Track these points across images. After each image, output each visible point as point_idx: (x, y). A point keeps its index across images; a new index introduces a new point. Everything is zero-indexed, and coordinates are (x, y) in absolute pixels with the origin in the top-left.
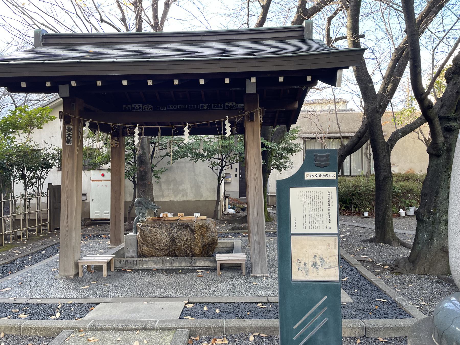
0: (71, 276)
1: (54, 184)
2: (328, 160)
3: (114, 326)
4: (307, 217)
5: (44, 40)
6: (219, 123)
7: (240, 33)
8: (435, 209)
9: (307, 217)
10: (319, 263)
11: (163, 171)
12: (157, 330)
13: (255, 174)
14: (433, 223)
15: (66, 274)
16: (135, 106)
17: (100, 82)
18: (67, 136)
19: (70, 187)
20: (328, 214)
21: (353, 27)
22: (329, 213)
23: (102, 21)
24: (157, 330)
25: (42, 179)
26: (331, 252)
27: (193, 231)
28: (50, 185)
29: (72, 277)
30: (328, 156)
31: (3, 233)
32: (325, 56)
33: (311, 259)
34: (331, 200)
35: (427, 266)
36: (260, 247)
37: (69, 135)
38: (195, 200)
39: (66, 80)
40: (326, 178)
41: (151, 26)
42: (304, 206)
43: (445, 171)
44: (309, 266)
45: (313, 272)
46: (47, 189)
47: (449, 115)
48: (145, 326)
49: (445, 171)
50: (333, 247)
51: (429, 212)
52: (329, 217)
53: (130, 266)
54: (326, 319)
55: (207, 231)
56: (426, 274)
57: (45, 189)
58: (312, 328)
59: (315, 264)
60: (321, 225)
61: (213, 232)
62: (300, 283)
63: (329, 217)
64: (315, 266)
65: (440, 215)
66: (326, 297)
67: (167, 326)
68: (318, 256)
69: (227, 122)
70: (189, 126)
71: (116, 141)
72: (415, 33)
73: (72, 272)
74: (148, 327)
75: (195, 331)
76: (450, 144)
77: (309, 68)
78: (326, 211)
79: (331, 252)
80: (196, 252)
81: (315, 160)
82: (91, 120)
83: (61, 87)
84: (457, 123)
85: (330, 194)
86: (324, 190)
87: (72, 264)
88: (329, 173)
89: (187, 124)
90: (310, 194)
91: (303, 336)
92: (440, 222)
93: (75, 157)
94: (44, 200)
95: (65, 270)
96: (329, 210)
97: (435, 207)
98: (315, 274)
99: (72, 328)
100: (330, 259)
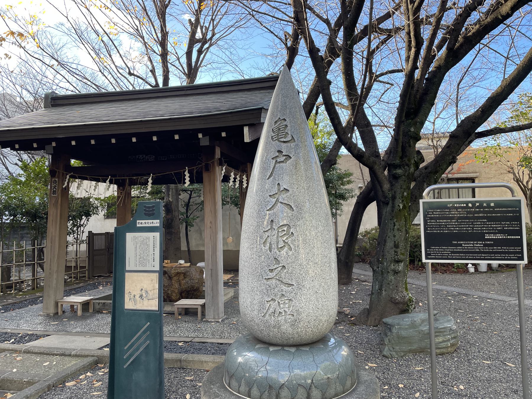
0: (51, 314)
1: (94, 232)
2: (153, 210)
3: (42, 350)
4: (138, 257)
5: (53, 101)
6: (180, 174)
7: (220, 85)
8: (383, 258)
9: (138, 257)
10: (144, 295)
11: (195, 219)
12: (73, 356)
13: (211, 222)
14: (382, 273)
15: (48, 312)
16: (139, 156)
17: (54, 143)
18: (53, 188)
19: (53, 234)
20: (153, 255)
21: (345, 71)
22: (154, 254)
23: (130, 74)
24: (73, 356)
25: (82, 227)
26: (154, 286)
27: (170, 278)
28: (90, 232)
29: (52, 315)
30: (153, 206)
31: (36, 277)
32: (229, 115)
33: (139, 292)
34: (155, 243)
35: (378, 318)
36: (213, 292)
37: (54, 187)
38: (235, 249)
39: (48, 141)
40: (152, 225)
41: (184, 74)
42: (136, 248)
43: (391, 219)
44: (137, 297)
45: (140, 303)
46: (87, 237)
47: (394, 162)
48: (65, 352)
49: (391, 219)
50: (155, 282)
51: (378, 260)
52: (154, 257)
53: (107, 308)
54: (148, 342)
55: (185, 278)
56: (377, 326)
57: (85, 236)
58: (138, 349)
59: (141, 296)
60: (147, 263)
61: (193, 280)
62: (130, 311)
63: (154, 257)
64: (141, 298)
65: (387, 264)
66: (149, 323)
67: (81, 354)
68: (144, 290)
69: (186, 173)
70: (152, 177)
71: (121, 190)
72: (325, 88)
73: (52, 311)
74: (66, 353)
75: (102, 359)
76: (395, 192)
77: (218, 126)
78: (151, 252)
79: (154, 286)
80: (173, 298)
81: (145, 210)
82: (72, 173)
83: (47, 147)
84: (402, 170)
85: (155, 238)
86: (151, 235)
87: (52, 304)
88: (154, 221)
89: (151, 174)
90: (140, 238)
91: (131, 356)
92: (388, 272)
93: (59, 207)
94: (84, 247)
95: (47, 309)
96: (154, 251)
97: (383, 256)
98: (141, 305)
99: (12, 350)
100: (152, 292)
